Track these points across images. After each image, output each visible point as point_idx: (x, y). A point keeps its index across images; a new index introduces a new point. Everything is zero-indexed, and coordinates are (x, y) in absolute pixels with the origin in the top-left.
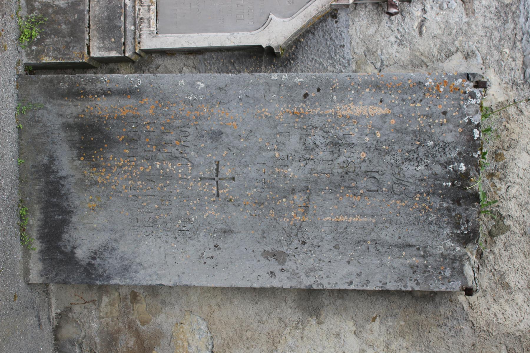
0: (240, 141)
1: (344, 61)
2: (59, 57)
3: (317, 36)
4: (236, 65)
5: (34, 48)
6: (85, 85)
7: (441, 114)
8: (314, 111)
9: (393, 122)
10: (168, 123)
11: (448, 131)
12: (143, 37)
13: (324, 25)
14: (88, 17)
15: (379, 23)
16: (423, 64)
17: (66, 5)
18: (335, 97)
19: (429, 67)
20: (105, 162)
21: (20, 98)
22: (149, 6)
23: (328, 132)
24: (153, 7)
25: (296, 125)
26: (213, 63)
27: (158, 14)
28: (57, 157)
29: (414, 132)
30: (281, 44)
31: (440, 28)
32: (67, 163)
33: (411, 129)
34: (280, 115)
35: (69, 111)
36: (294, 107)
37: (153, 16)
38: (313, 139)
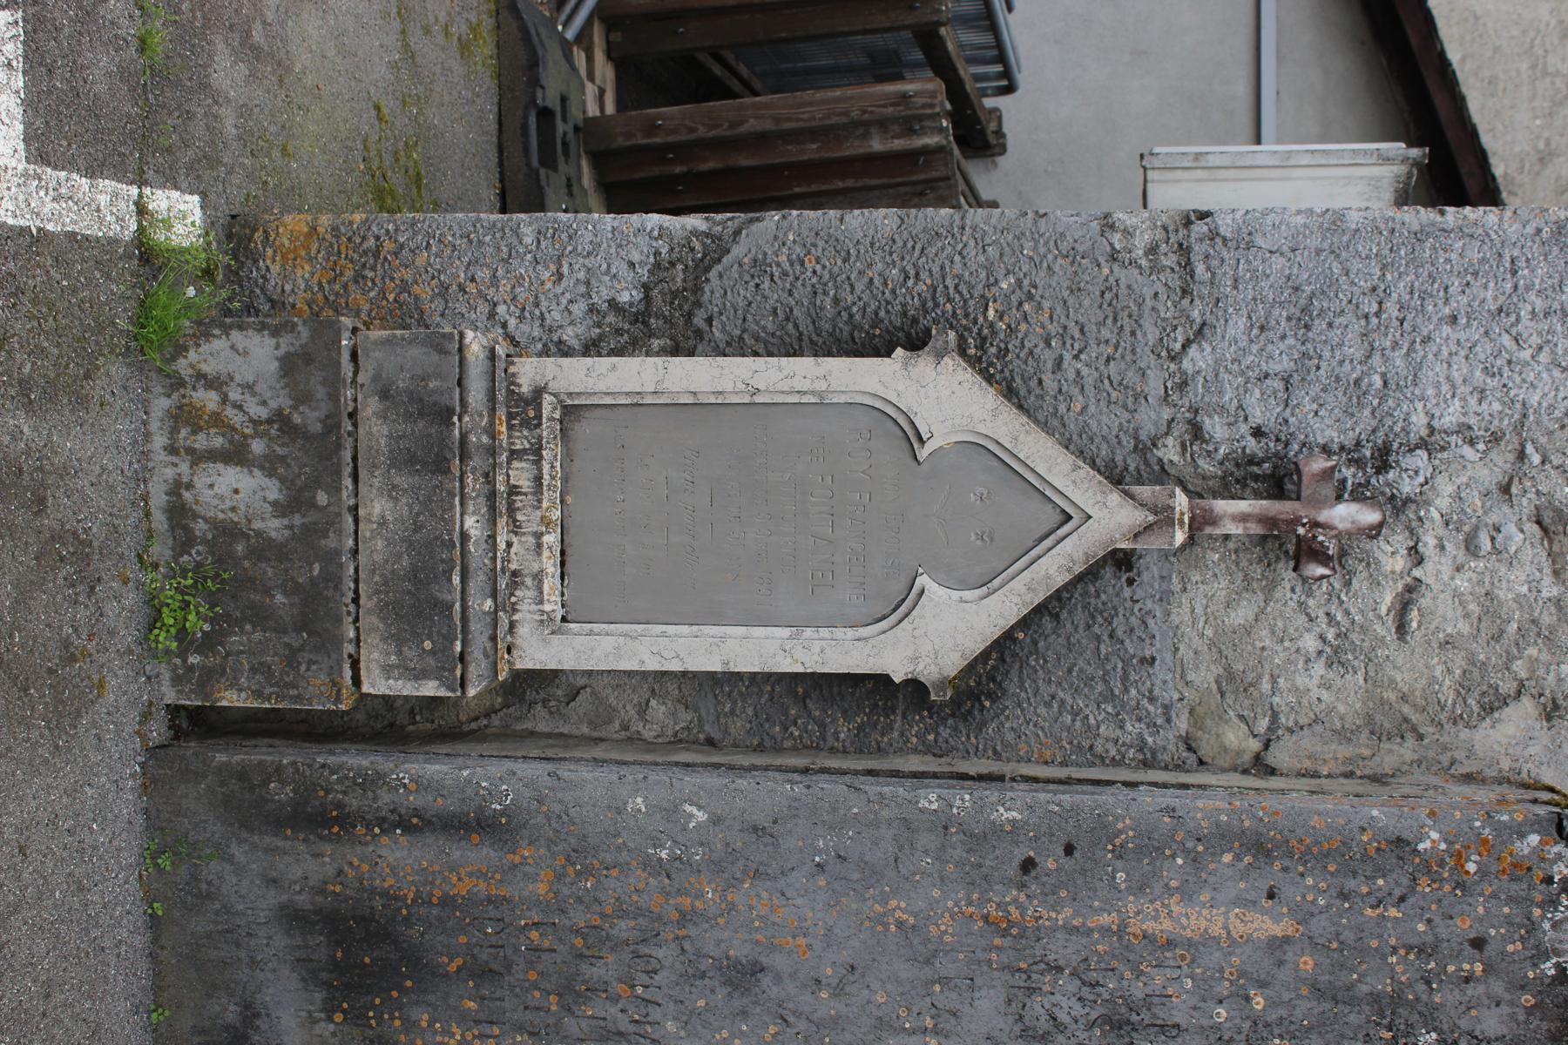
0: (817, 998)
1: (1151, 708)
2: (268, 690)
3: (1068, 626)
4: (810, 705)
5: (194, 659)
6: (344, 793)
7: (1467, 946)
8: (1053, 915)
9: (1307, 963)
10: (595, 927)
11: (1487, 1002)
12: (523, 631)
13: (1092, 589)
14: (352, 571)
15: (1269, 591)
16: (1406, 729)
17: (287, 533)
18: (1121, 876)
19: (1426, 741)
20: (407, 1031)
21: (154, 822)
22: (538, 536)
23: (1097, 983)
24: (551, 539)
25: (994, 956)
26: (741, 693)
27: (568, 559)
28: (266, 1008)
29: (1375, 999)
30: (951, 362)
31: (1467, 616)
33: (1365, 988)
34: (945, 923)
35: (296, 872)
36: (990, 900)
37: (550, 566)
38: (1047, 1006)
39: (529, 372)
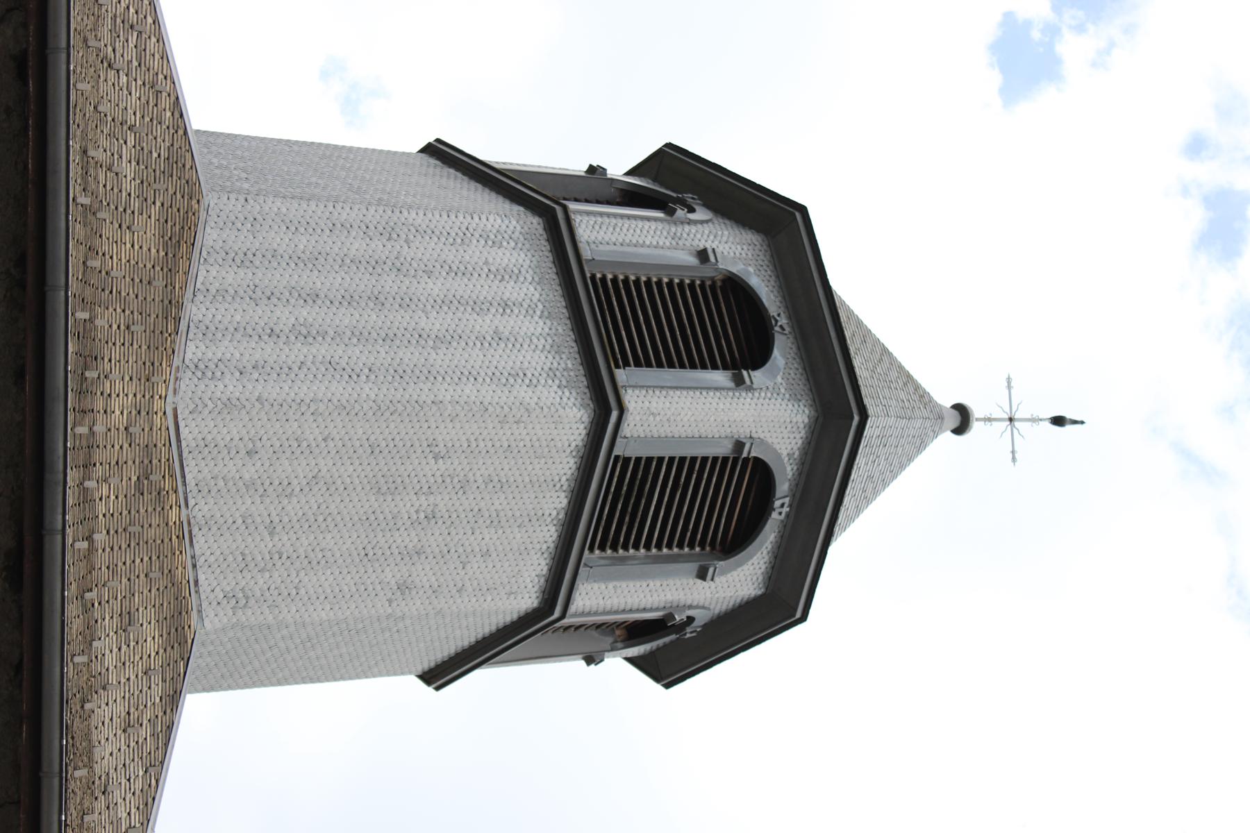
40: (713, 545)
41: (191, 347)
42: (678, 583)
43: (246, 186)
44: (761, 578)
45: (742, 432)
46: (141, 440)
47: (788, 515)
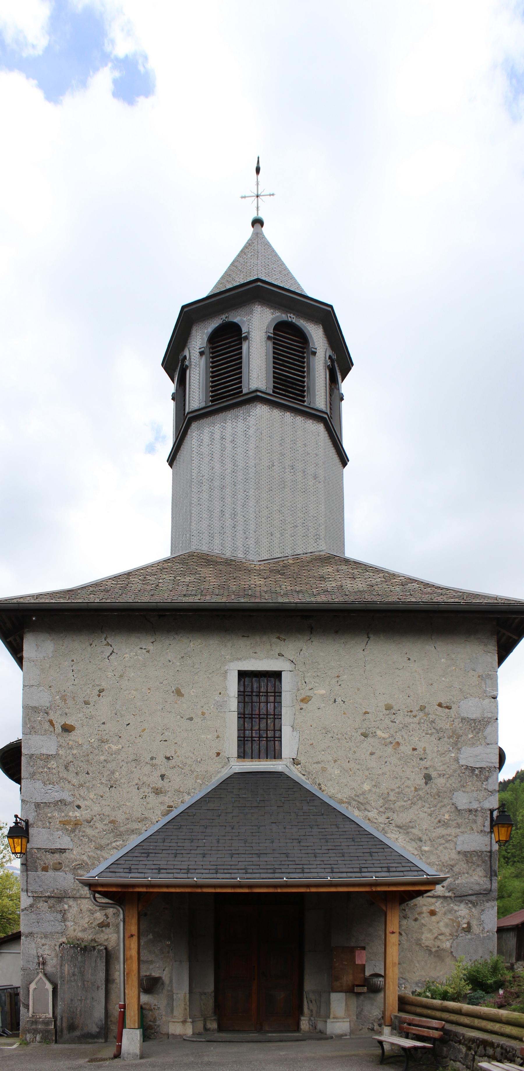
32: (77, 1033)
39: (30, 1016)
40: (303, 348)
41: (239, 555)
42: (317, 364)
43: (188, 535)
44: (316, 326)
45: (264, 336)
46: (268, 573)
47: (294, 314)
